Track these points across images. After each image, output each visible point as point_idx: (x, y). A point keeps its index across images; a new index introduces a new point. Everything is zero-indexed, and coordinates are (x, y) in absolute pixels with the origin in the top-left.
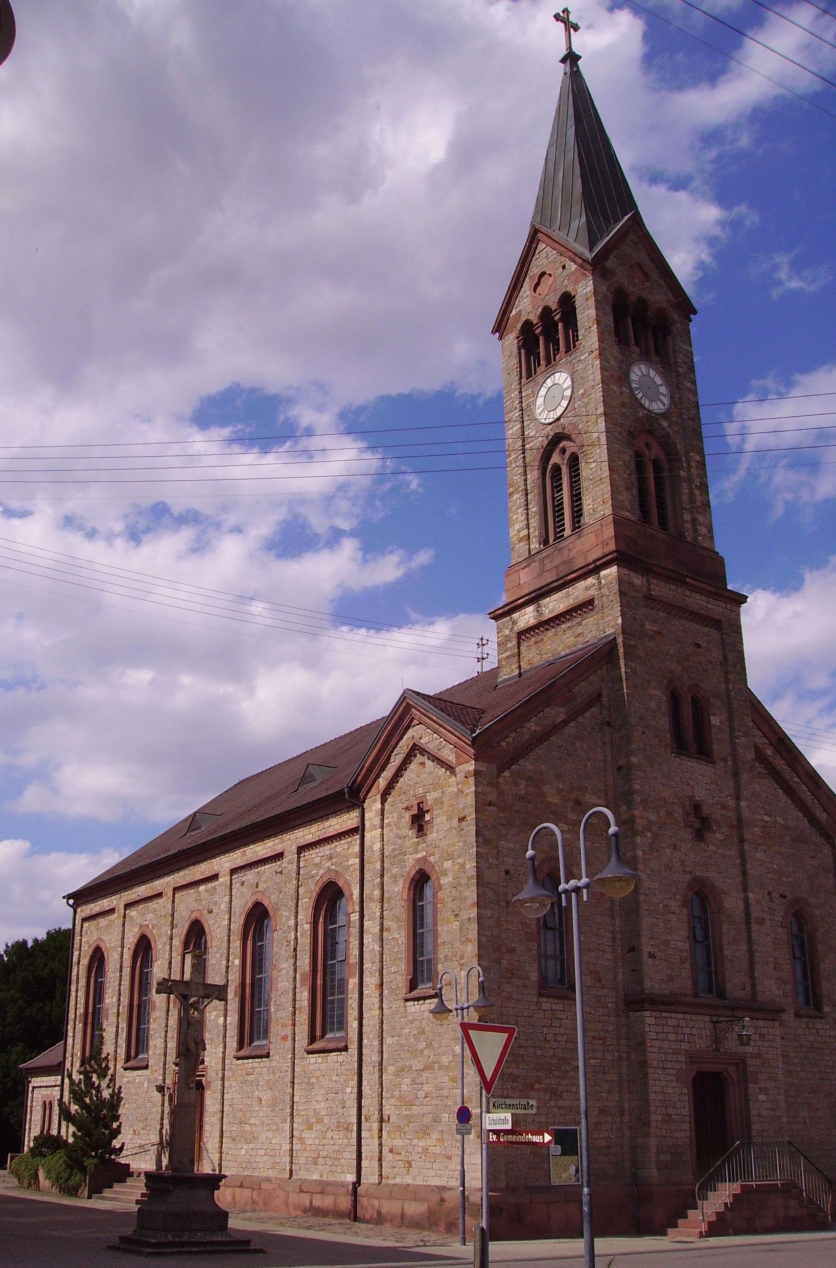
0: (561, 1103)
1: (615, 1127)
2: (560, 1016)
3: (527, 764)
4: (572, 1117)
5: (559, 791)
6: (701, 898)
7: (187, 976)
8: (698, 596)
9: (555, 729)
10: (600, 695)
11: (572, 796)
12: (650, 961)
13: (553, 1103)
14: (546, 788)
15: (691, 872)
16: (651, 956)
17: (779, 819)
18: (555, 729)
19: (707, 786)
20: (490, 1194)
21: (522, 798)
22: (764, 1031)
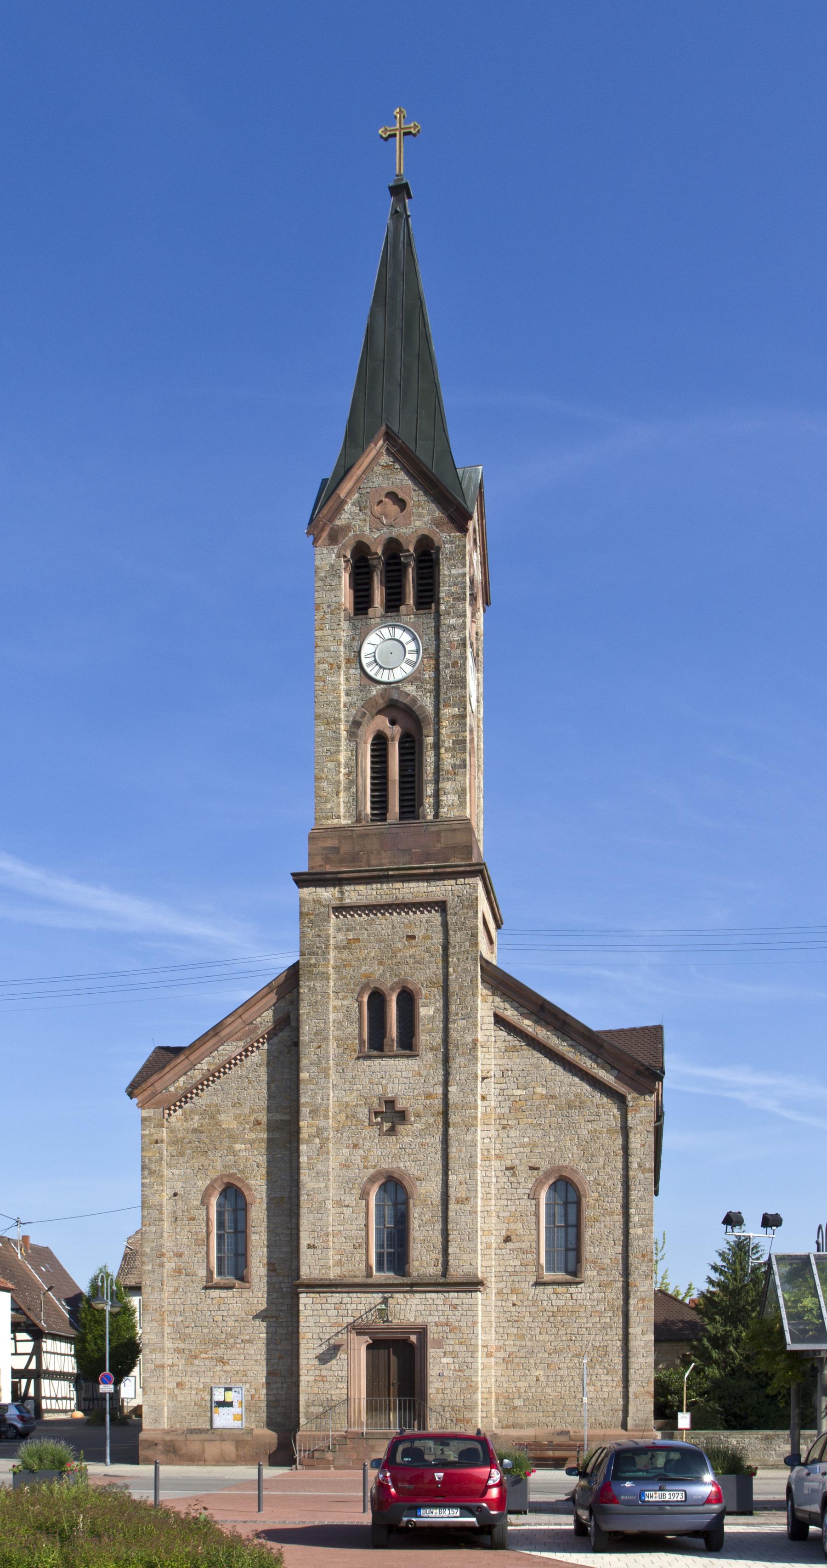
0: (227, 1368)
1: (285, 1386)
2: (229, 1302)
3: (203, 1100)
4: (238, 1379)
5: (236, 1117)
6: (395, 1190)
7: (47, 1417)
8: (413, 885)
9: (230, 1063)
10: (289, 1017)
11: (252, 1119)
12: (311, 1251)
13: (218, 1368)
14: (222, 1117)
15: (375, 1166)
16: (309, 1246)
17: (539, 1090)
18: (230, 1063)
19: (406, 1081)
20: (108, 1395)
21: (195, 1131)
22: (455, 1301)
